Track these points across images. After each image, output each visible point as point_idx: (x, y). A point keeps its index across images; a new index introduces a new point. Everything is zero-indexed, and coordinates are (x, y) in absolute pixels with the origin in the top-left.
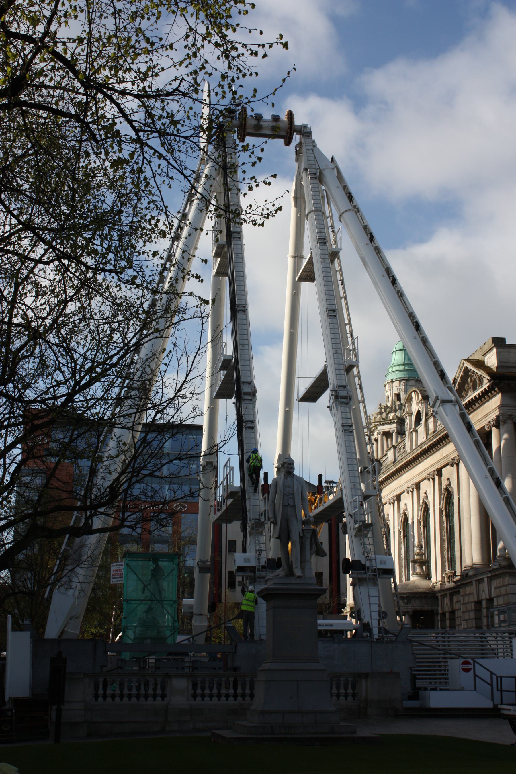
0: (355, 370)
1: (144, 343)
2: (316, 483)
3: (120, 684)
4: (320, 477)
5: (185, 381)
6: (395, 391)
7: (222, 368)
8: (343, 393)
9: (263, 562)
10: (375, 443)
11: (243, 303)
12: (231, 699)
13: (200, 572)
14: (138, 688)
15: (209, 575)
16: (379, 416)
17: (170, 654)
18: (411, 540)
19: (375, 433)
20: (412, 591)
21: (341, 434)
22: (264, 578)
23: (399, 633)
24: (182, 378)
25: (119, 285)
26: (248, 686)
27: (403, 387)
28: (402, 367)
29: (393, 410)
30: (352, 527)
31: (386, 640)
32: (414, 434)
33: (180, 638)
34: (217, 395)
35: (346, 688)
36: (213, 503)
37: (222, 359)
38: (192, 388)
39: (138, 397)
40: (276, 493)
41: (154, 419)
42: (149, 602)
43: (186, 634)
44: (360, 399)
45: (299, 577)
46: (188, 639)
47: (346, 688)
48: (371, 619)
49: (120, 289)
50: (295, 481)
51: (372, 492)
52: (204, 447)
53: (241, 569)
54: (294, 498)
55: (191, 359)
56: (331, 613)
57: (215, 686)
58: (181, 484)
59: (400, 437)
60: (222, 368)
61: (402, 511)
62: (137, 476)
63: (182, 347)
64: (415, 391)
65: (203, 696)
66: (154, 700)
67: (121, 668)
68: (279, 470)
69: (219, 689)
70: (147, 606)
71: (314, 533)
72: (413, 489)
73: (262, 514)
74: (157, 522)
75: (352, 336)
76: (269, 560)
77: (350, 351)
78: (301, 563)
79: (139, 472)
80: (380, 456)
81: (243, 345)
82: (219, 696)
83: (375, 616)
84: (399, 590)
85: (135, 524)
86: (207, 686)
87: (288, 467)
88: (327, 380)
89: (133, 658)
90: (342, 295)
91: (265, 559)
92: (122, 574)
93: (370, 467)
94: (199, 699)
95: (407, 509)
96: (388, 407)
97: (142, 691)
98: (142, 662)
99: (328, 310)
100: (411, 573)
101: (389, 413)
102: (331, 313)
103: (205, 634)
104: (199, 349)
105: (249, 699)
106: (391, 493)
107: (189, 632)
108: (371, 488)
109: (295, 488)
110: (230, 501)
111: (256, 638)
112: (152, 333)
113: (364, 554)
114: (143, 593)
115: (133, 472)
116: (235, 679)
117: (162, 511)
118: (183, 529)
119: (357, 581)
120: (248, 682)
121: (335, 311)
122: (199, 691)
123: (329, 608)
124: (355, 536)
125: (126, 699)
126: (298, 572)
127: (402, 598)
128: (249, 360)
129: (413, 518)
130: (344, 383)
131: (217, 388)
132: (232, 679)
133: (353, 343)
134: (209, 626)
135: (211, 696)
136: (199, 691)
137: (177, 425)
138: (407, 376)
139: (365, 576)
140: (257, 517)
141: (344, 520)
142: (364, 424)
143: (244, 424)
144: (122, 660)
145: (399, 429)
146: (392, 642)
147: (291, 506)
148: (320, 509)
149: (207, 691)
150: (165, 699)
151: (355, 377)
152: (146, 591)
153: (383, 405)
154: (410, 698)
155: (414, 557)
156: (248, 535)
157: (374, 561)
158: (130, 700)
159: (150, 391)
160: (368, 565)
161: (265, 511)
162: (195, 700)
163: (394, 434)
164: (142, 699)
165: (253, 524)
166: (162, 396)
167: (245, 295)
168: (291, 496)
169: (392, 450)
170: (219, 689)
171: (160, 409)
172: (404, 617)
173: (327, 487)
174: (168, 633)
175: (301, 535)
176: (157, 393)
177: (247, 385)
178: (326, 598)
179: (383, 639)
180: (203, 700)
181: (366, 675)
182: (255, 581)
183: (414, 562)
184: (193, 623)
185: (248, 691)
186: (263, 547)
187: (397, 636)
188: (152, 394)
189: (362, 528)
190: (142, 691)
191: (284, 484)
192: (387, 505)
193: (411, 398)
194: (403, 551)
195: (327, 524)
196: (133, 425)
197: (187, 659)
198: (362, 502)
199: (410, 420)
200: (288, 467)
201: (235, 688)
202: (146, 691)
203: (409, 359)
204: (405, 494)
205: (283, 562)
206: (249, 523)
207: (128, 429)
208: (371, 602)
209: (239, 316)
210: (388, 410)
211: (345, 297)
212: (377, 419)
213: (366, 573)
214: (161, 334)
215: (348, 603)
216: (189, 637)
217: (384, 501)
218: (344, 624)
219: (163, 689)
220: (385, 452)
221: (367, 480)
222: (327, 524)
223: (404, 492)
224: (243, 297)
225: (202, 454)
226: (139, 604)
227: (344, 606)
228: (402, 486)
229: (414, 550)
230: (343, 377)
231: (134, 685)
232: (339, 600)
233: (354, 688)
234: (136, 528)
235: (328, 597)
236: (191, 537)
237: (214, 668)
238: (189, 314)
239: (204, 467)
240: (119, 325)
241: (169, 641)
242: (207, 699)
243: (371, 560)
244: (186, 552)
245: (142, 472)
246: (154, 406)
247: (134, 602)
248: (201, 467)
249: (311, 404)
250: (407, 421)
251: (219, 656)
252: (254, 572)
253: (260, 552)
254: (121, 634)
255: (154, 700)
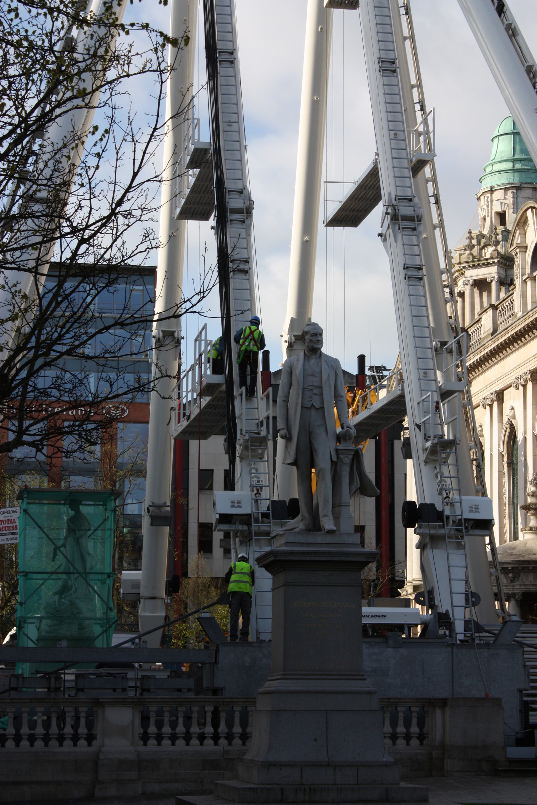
0: (427, 170)
1: (57, 117)
2: (354, 371)
3: (15, 718)
4: (362, 359)
5: (130, 187)
6: (497, 208)
7: (192, 164)
8: (405, 210)
9: (264, 507)
10: (460, 300)
11: (229, 46)
12: (209, 742)
13: (152, 525)
14: (47, 725)
15: (167, 529)
16: (468, 252)
17: (101, 665)
18: (521, 469)
19: (460, 283)
20: (522, 559)
21: (403, 283)
22: (268, 534)
23: (500, 631)
24: (124, 180)
25: (16, 9)
26: (237, 721)
27: (510, 201)
28: (509, 165)
29: (491, 242)
30: (420, 447)
31: (477, 642)
32: (529, 283)
33: (117, 639)
34: (181, 213)
35: (408, 725)
36: (174, 404)
37: (192, 148)
38: (141, 200)
39: (46, 215)
40: (291, 385)
41: (75, 254)
42: (64, 576)
43: (131, 631)
44: (436, 221)
45: (331, 532)
46: (132, 640)
47: (408, 725)
48: (453, 606)
49: (17, 15)
50: (323, 363)
51: (454, 385)
52: (159, 307)
53: (225, 518)
54: (321, 394)
55: (140, 148)
56: (378, 595)
57: (181, 720)
58: (119, 370)
59: (503, 289)
60: (192, 164)
61: (505, 420)
62: (47, 354)
63: (124, 124)
64: (532, 208)
65: (159, 738)
66: (75, 745)
67: (15, 689)
68: (290, 346)
69: (187, 725)
70: (60, 583)
71: (357, 456)
72: (526, 381)
73: (262, 422)
74: (80, 436)
75: (422, 108)
76: (274, 502)
77: (420, 134)
78: (333, 507)
79: (49, 348)
80: (467, 323)
81: (229, 123)
82: (188, 738)
83: (460, 600)
84: (500, 557)
85: (40, 440)
86: (166, 719)
87: (311, 341)
88: (379, 188)
89: (38, 672)
90: (406, 33)
91: (268, 502)
92: (16, 527)
93: (452, 342)
94: (152, 742)
95: (514, 417)
96: (483, 236)
97: (54, 729)
98: (53, 680)
99: (382, 61)
100: (520, 526)
101: (485, 246)
102: (388, 66)
103: (161, 631)
104: (155, 129)
105: (240, 742)
106: (486, 387)
107: (133, 627)
108: (454, 378)
109: (325, 377)
110: (205, 400)
111: (251, 638)
112: (70, 99)
113: (440, 494)
114: (53, 560)
115: (37, 347)
116: (216, 708)
117: (87, 418)
118: (119, 450)
119: (428, 540)
120: (237, 714)
121: (393, 63)
122: (152, 729)
123: (375, 586)
124: (426, 462)
125: (25, 743)
126: (328, 524)
127: (505, 571)
128: (240, 151)
129: (525, 432)
130: (408, 193)
131: (183, 201)
132: (210, 709)
133: (425, 122)
134: (166, 617)
135: (173, 738)
136: (152, 729)
137: (117, 266)
138: (517, 180)
139: (441, 531)
140: (254, 428)
141: (405, 434)
142: (443, 266)
143: (231, 265)
144: (17, 677)
145: (503, 276)
146: (487, 645)
147: (317, 409)
148: (363, 414)
149: (167, 730)
150: (94, 742)
151: (427, 181)
152: (60, 557)
153: (475, 232)
154: (519, 743)
155: (526, 499)
156: (238, 460)
157: (457, 506)
158: (32, 745)
159: (65, 204)
160: (447, 512)
161: (268, 418)
162: (145, 744)
163: (493, 284)
164: (54, 743)
165: (247, 441)
166: (90, 213)
167: (233, 32)
168: (316, 391)
169: (490, 312)
170: (187, 725)
171: (86, 237)
172: (507, 603)
173: (373, 377)
174: (97, 629)
175: (335, 459)
176: (80, 207)
177: (236, 196)
178: (370, 570)
179: (473, 640)
180: (159, 744)
181: (443, 703)
182: (250, 540)
183: (527, 508)
184: (141, 612)
185: (237, 729)
186: (265, 480)
187: (497, 636)
188: (69, 209)
189: (438, 448)
190: (54, 729)
191: (304, 370)
192: (480, 408)
193: (526, 219)
194: (506, 489)
195: (373, 441)
196: (38, 265)
197: (131, 674)
198: (437, 403)
199: (524, 260)
200: (311, 341)
201: (216, 724)
202: (61, 729)
203: (525, 151)
204: (512, 389)
205: (302, 506)
206: (240, 440)
207: (29, 270)
208: (452, 577)
209: (221, 70)
210: (483, 241)
211: (412, 38)
212: (464, 258)
213: (443, 527)
214: (87, 101)
215: (409, 578)
216: (132, 636)
217: (475, 402)
218: (405, 614)
219: (90, 725)
220: (477, 317)
221: (447, 365)
222: (373, 441)
223: (510, 386)
224: (229, 36)
225: (156, 317)
226: (45, 580)
227: (402, 584)
228: (506, 375)
229: (525, 488)
230: (407, 182)
231: (39, 718)
232: (393, 574)
233: (421, 724)
234: (43, 446)
235: (374, 569)
236: (135, 464)
237: (179, 690)
238: (137, 64)
239: (158, 341)
240: (10, 83)
241: (99, 643)
242: (166, 742)
243: (452, 504)
244: (126, 490)
245: (57, 347)
246: (74, 231)
247: (35, 576)
248: (154, 340)
249: (348, 229)
250: (518, 261)
251: (184, 669)
252: (249, 524)
253: (258, 489)
254: (13, 631)
255: (75, 745)
